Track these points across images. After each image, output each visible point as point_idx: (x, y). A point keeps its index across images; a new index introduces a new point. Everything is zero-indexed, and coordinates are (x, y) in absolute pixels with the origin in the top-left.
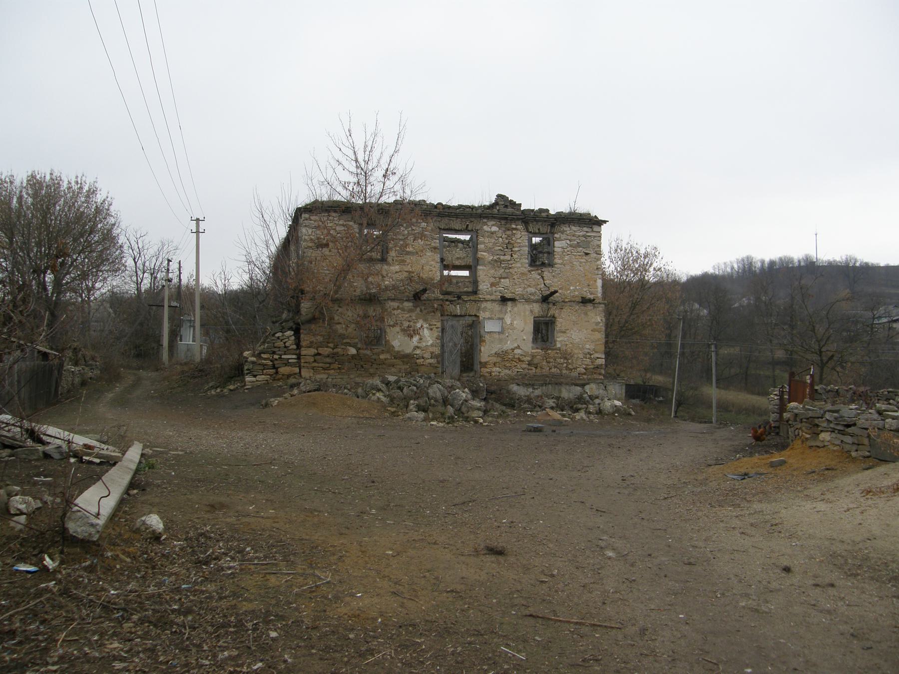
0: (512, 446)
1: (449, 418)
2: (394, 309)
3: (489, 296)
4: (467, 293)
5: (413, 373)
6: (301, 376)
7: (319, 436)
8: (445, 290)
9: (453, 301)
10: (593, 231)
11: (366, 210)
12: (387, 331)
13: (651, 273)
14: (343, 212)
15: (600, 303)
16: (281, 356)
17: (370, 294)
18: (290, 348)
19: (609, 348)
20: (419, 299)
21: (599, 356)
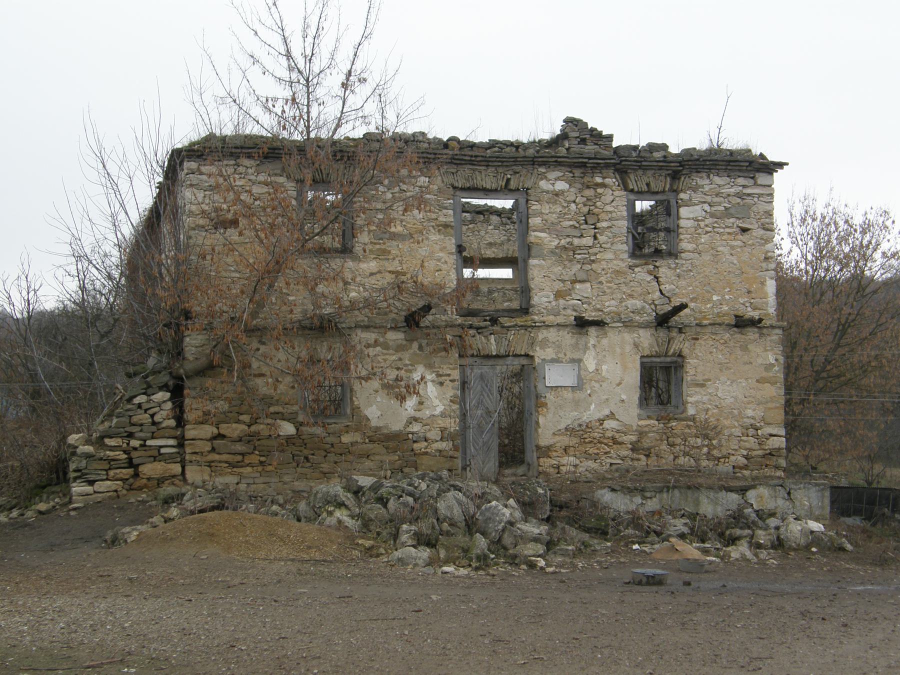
0: (604, 614)
1: (478, 558)
2: (368, 346)
3: (551, 318)
4: (511, 312)
5: (406, 470)
6: (185, 480)
7: (221, 601)
8: (465, 306)
9: (482, 328)
10: (755, 184)
11: (310, 154)
12: (355, 388)
13: (878, 263)
14: (266, 158)
15: (772, 327)
16: (145, 441)
17: (321, 317)
18: (164, 425)
19: (794, 415)
20: (417, 325)
21: (774, 432)
